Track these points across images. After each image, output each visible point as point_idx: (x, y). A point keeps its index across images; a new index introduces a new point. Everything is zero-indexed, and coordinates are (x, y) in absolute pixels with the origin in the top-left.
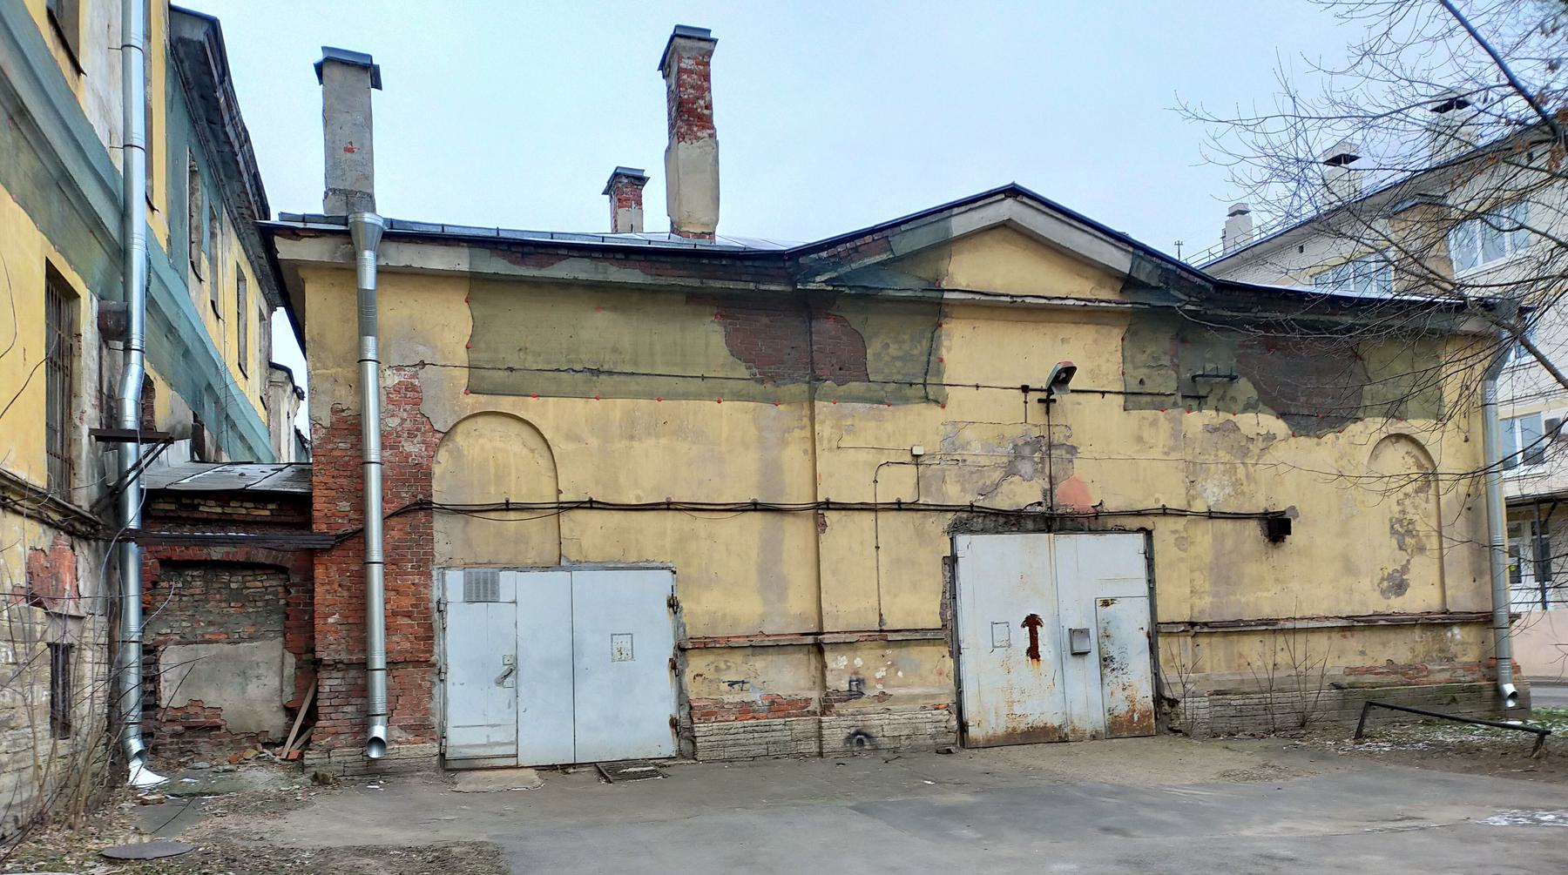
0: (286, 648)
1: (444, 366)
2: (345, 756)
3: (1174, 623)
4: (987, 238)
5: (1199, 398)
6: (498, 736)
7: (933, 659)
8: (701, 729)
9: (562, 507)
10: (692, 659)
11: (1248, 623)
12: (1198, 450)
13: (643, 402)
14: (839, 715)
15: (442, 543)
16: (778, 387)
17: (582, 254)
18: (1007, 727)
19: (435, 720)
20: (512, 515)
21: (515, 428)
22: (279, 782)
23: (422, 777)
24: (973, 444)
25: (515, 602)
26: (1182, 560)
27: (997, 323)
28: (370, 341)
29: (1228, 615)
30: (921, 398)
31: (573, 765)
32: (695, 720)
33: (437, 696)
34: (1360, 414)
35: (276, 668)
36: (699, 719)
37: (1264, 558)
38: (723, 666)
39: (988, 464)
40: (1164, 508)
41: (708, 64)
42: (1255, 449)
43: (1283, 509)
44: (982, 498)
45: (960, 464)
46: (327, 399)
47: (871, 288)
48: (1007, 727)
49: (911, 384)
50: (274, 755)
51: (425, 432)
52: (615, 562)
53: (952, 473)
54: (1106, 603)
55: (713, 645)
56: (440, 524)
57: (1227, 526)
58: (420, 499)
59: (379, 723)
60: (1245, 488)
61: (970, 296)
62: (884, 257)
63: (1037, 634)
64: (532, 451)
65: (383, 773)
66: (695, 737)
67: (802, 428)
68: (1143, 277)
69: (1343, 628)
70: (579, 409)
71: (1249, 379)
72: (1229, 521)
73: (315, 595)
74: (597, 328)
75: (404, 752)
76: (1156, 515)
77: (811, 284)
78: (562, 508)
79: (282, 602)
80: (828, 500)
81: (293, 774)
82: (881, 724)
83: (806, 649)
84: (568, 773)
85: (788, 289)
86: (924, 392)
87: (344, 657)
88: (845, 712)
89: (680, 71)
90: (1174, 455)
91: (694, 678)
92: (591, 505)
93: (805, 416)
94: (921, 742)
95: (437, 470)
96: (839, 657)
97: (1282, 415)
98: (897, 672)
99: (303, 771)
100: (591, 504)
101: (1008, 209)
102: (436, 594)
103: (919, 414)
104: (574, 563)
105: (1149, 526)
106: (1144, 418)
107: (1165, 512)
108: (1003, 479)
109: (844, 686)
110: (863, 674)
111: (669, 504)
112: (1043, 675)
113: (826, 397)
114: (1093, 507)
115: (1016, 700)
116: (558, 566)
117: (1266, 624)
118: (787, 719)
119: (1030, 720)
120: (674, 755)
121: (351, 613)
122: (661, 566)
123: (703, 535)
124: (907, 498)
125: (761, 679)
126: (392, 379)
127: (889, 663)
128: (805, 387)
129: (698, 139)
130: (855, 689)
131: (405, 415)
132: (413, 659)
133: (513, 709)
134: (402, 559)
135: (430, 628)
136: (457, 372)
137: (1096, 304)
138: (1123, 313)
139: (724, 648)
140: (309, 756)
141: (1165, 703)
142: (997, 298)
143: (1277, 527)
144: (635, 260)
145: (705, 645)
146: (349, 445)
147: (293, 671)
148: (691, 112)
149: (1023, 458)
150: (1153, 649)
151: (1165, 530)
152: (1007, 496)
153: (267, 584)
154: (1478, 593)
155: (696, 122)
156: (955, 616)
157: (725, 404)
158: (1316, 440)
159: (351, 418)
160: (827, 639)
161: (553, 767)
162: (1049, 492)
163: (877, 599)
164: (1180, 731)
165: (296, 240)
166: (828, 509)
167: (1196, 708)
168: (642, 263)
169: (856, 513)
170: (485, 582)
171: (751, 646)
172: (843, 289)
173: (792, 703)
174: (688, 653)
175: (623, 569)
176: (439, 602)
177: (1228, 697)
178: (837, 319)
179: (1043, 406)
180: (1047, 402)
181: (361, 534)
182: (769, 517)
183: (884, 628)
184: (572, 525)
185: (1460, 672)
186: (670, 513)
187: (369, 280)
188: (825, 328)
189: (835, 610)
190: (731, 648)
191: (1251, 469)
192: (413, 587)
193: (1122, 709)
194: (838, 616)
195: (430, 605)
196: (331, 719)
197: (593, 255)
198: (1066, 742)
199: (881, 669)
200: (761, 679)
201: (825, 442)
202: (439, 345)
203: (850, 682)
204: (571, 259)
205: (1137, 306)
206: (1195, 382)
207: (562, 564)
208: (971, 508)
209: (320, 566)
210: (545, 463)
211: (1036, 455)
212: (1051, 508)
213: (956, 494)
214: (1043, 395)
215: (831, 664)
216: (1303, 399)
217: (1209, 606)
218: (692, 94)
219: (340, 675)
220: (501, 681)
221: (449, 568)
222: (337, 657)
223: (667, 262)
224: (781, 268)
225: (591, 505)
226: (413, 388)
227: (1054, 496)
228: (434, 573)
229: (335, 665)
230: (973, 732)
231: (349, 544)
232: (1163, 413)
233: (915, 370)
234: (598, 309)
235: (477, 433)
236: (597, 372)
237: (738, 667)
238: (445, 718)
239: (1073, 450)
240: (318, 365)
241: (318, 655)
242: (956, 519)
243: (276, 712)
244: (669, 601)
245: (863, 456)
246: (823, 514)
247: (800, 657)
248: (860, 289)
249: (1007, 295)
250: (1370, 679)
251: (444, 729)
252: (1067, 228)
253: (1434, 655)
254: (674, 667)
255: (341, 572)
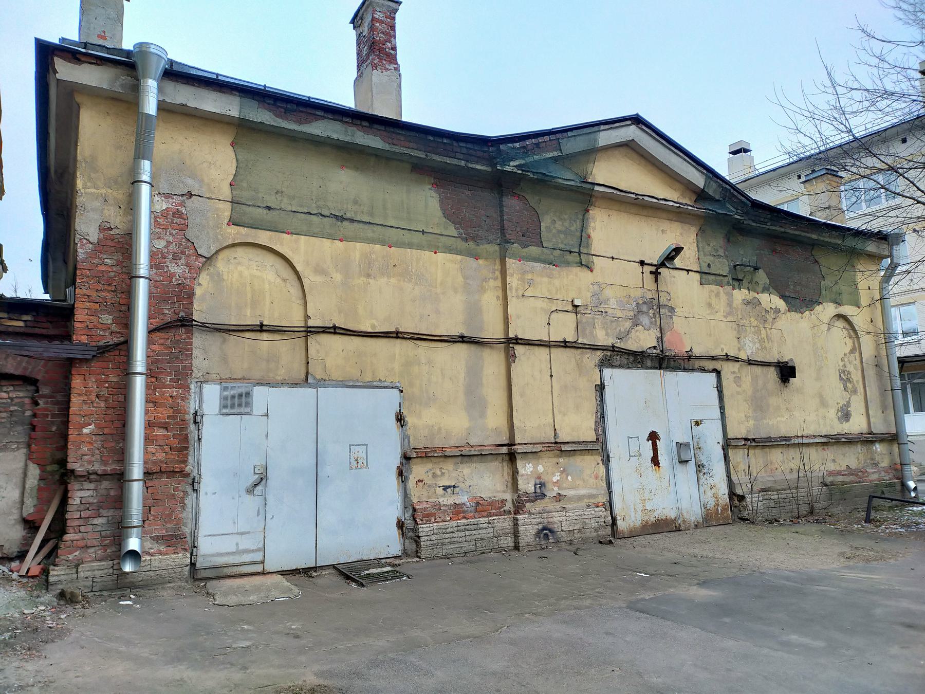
0: (30, 459)
1: (209, 198)
2: (94, 570)
3: (737, 439)
4: (617, 152)
5: (739, 280)
6: (246, 543)
7: (590, 465)
8: (424, 529)
9: (310, 331)
10: (414, 467)
11: (776, 439)
12: (740, 316)
13: (377, 247)
14: (530, 514)
15: (201, 358)
16: (478, 245)
17: (336, 117)
18: (643, 520)
19: (187, 530)
20: (265, 336)
21: (271, 259)
22: (21, 603)
23: (173, 588)
24: (611, 300)
25: (267, 415)
26: (738, 393)
27: (623, 214)
28: (146, 165)
29: (763, 434)
30: (577, 263)
31: (315, 569)
32: (419, 521)
33: (189, 505)
34: (820, 300)
35: (17, 479)
36: (421, 520)
37: (780, 394)
38: (439, 473)
39: (622, 316)
40: (727, 355)
41: (394, 19)
42: (770, 317)
43: (787, 361)
44: (619, 341)
45: (604, 314)
46: (96, 217)
47: (548, 176)
48: (643, 520)
49: (571, 252)
50: (11, 571)
51: (189, 256)
52: (353, 381)
53: (599, 320)
54: (697, 424)
55: (432, 454)
56: (198, 340)
57: (758, 370)
58: (182, 316)
59: (134, 535)
60: (766, 344)
61: (611, 191)
62: (555, 154)
63: (657, 446)
64: (285, 280)
65: (133, 586)
66: (419, 537)
67: (495, 279)
68: (711, 193)
69: (824, 444)
70: (327, 248)
71: (764, 271)
72: (759, 367)
73: (71, 405)
74: (341, 183)
75: (156, 564)
76: (722, 360)
77: (507, 167)
78: (310, 332)
79: (28, 413)
80: (516, 336)
81: (35, 593)
82: (561, 520)
83: (500, 458)
84: (311, 577)
85: (489, 169)
86: (579, 259)
87: (98, 467)
88: (534, 511)
89: (373, 19)
90: (729, 319)
91: (417, 484)
92: (334, 330)
93: (497, 270)
94: (588, 534)
95: (198, 291)
96: (527, 465)
97: (782, 297)
98: (567, 477)
99: (47, 589)
100: (335, 329)
101: (631, 132)
102: (193, 406)
103: (576, 275)
104: (319, 380)
105: (719, 368)
106: (712, 291)
107: (727, 358)
108: (632, 328)
109: (531, 489)
110: (545, 478)
111: (397, 333)
112: (663, 479)
113: (513, 256)
114: (686, 352)
115: (647, 498)
116: (306, 381)
117: (785, 440)
118: (490, 518)
119: (656, 514)
120: (400, 554)
121: (107, 423)
122: (391, 386)
123: (423, 360)
124: (570, 338)
125: (468, 484)
126: (162, 205)
127: (562, 469)
128: (497, 248)
129: (387, 69)
130: (538, 491)
131: (171, 239)
132: (168, 469)
133: (261, 516)
134: (162, 373)
135: (186, 438)
136: (221, 205)
137: (686, 207)
138: (698, 216)
139: (440, 457)
140: (55, 573)
141: (736, 499)
142: (627, 195)
143: (786, 372)
144: (377, 129)
145: (426, 455)
146: (115, 262)
147: (36, 482)
148: (381, 50)
149: (643, 313)
150: (726, 457)
151: (728, 369)
152: (635, 340)
153: (13, 395)
154: (886, 420)
155: (385, 58)
156: (604, 431)
157: (440, 255)
158: (800, 315)
159: (118, 236)
160: (520, 449)
161: (296, 572)
162: (661, 339)
163: (552, 416)
164: (747, 520)
165: (77, 64)
166: (517, 343)
167: (754, 502)
168: (382, 132)
169: (536, 347)
170: (240, 395)
171: (461, 455)
172: (529, 174)
173: (492, 504)
174: (412, 462)
175: (360, 387)
176: (195, 414)
177: (770, 493)
178: (518, 196)
179: (653, 276)
180: (656, 274)
181: (125, 346)
182: (473, 348)
183: (558, 440)
184: (318, 347)
185: (883, 474)
186: (399, 341)
187: (150, 106)
188: (512, 204)
189: (523, 425)
190: (446, 457)
191: (769, 332)
192: (170, 399)
193: (711, 504)
194: (525, 431)
195: (187, 417)
196: (80, 532)
197: (344, 119)
198: (680, 531)
199: (557, 474)
200: (468, 484)
201: (514, 291)
202: (206, 180)
203: (535, 485)
204: (326, 120)
205: (709, 211)
206: (736, 269)
207: (309, 381)
208: (613, 348)
209: (77, 376)
210: (295, 291)
211: (651, 311)
212: (662, 351)
213: (603, 337)
214: (653, 269)
215: (521, 471)
216: (792, 287)
217: (752, 427)
218: (383, 37)
219: (92, 486)
220: (251, 490)
221: (206, 382)
222: (90, 468)
223: (402, 134)
224: (485, 152)
225: (334, 330)
226: (178, 214)
227: (663, 343)
228: (192, 387)
229: (87, 477)
230: (621, 525)
231: (109, 356)
232: (722, 288)
233: (573, 242)
234: (342, 167)
235: (236, 261)
236: (342, 219)
237: (450, 473)
238: (196, 526)
239: (672, 310)
240: (89, 184)
241: (70, 466)
242: (603, 356)
243: (14, 525)
244: (397, 416)
245: (540, 304)
246: (513, 347)
247: (495, 465)
248: (540, 175)
249: (633, 193)
250: (840, 479)
251: (195, 538)
252: (668, 151)
253: (868, 461)
254: (400, 473)
255: (99, 383)
